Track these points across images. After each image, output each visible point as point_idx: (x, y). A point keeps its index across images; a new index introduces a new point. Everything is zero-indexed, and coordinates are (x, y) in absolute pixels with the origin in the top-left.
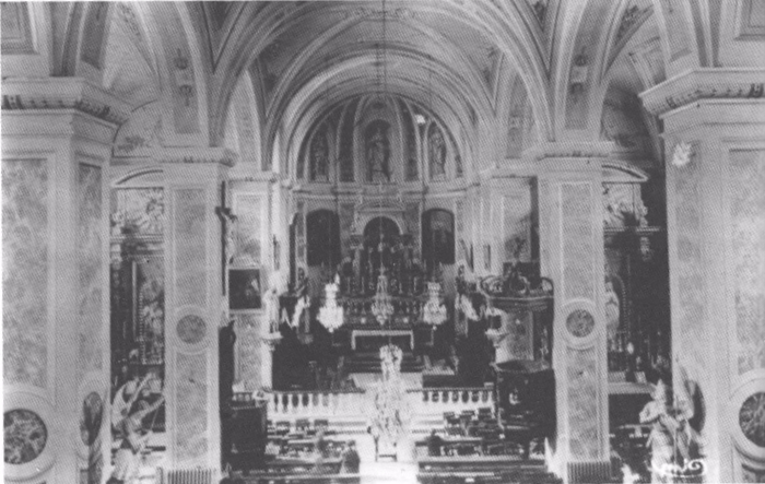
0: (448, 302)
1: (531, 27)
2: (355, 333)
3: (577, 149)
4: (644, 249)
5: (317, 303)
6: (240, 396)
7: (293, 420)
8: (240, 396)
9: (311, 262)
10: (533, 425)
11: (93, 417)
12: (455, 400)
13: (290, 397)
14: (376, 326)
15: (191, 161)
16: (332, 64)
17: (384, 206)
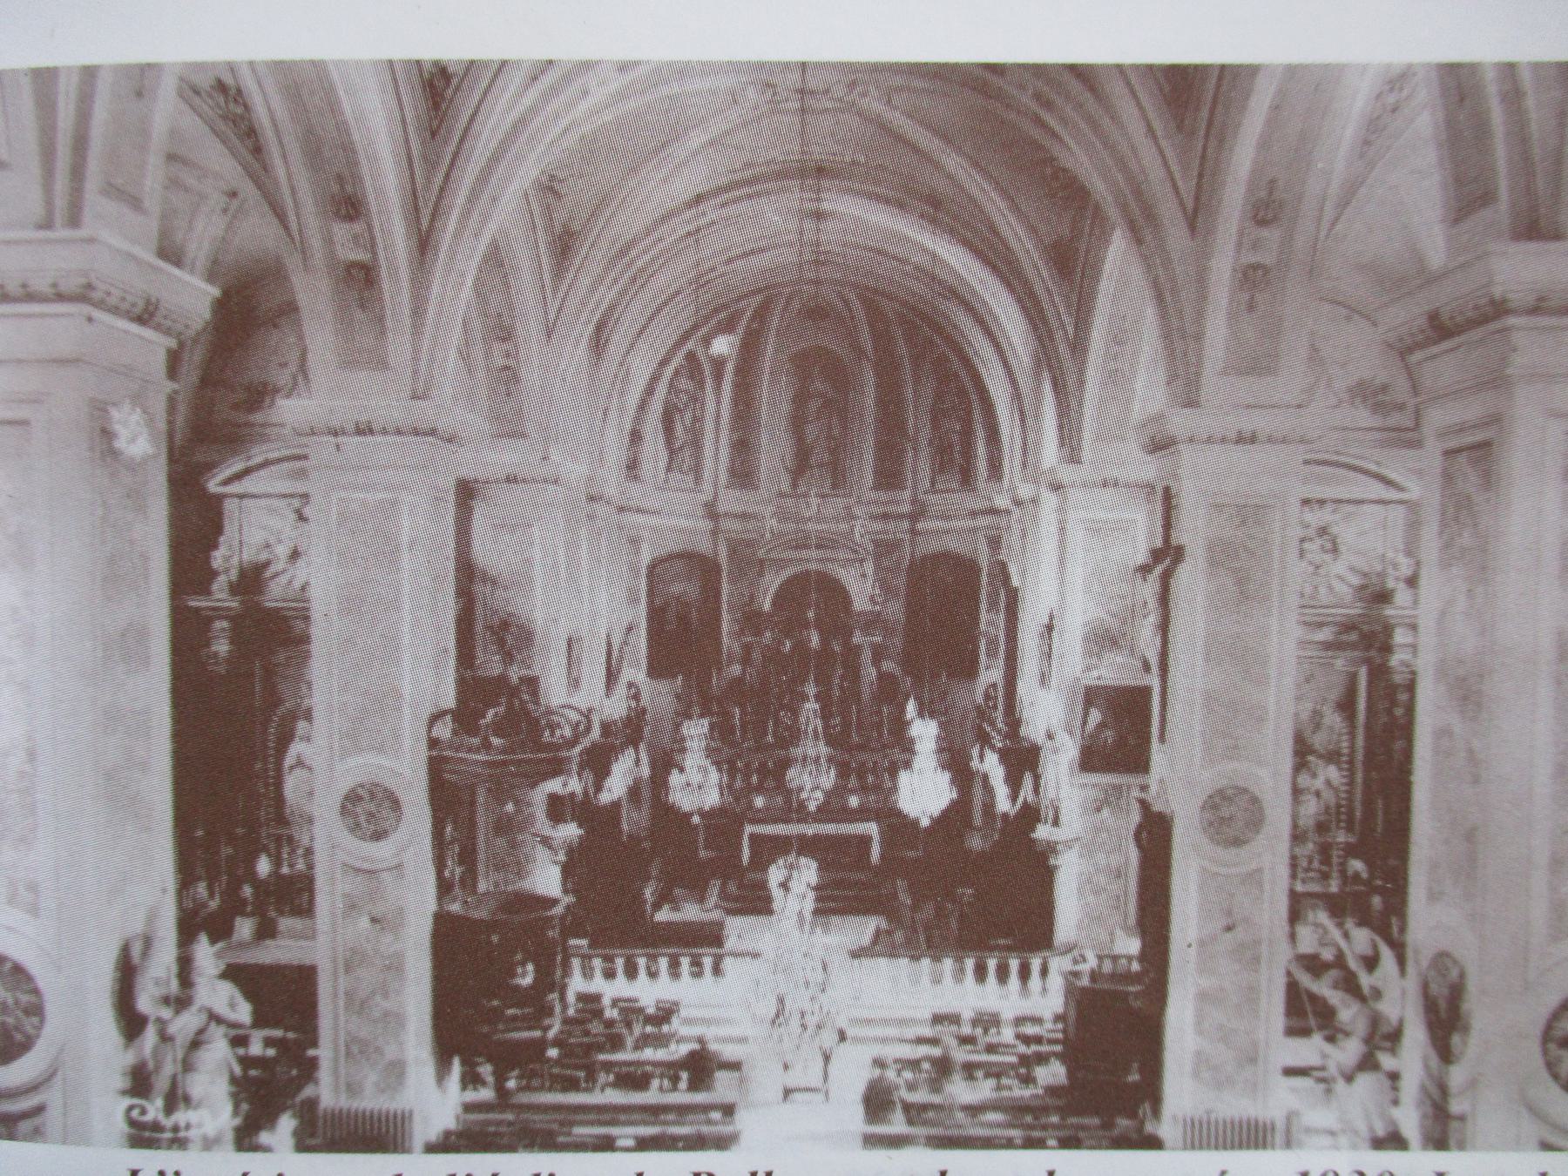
0: (956, 763)
1: (410, 115)
2: (749, 829)
3: (364, 418)
4: (222, 647)
5: (665, 763)
6: (1124, 961)
7: (1008, 1014)
8: (1124, 961)
9: (656, 669)
10: (485, 1029)
11: (1443, 1004)
12: (698, 974)
13: (992, 964)
14: (802, 815)
15: (1253, 439)
16: (425, 90)
17: (818, 547)
